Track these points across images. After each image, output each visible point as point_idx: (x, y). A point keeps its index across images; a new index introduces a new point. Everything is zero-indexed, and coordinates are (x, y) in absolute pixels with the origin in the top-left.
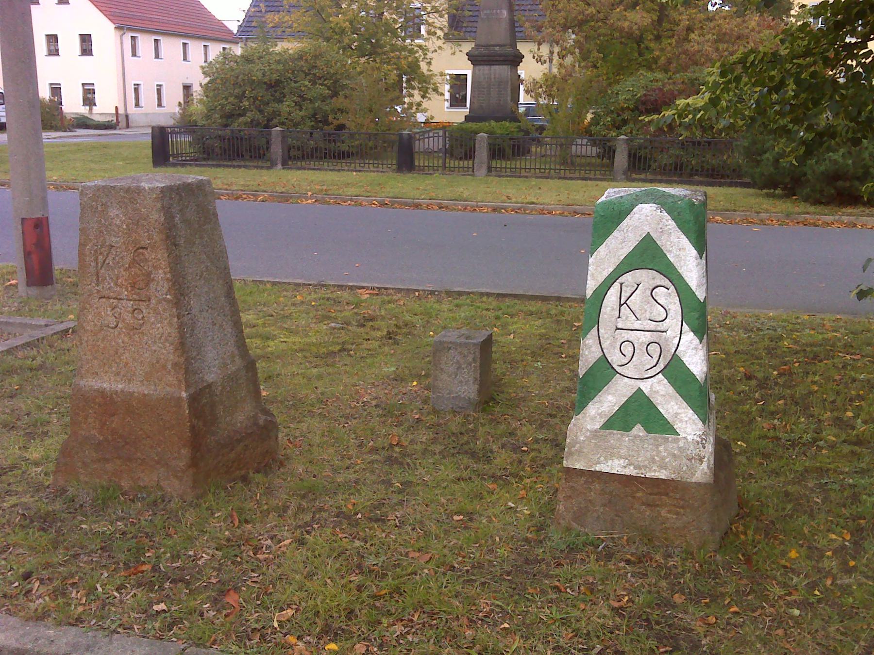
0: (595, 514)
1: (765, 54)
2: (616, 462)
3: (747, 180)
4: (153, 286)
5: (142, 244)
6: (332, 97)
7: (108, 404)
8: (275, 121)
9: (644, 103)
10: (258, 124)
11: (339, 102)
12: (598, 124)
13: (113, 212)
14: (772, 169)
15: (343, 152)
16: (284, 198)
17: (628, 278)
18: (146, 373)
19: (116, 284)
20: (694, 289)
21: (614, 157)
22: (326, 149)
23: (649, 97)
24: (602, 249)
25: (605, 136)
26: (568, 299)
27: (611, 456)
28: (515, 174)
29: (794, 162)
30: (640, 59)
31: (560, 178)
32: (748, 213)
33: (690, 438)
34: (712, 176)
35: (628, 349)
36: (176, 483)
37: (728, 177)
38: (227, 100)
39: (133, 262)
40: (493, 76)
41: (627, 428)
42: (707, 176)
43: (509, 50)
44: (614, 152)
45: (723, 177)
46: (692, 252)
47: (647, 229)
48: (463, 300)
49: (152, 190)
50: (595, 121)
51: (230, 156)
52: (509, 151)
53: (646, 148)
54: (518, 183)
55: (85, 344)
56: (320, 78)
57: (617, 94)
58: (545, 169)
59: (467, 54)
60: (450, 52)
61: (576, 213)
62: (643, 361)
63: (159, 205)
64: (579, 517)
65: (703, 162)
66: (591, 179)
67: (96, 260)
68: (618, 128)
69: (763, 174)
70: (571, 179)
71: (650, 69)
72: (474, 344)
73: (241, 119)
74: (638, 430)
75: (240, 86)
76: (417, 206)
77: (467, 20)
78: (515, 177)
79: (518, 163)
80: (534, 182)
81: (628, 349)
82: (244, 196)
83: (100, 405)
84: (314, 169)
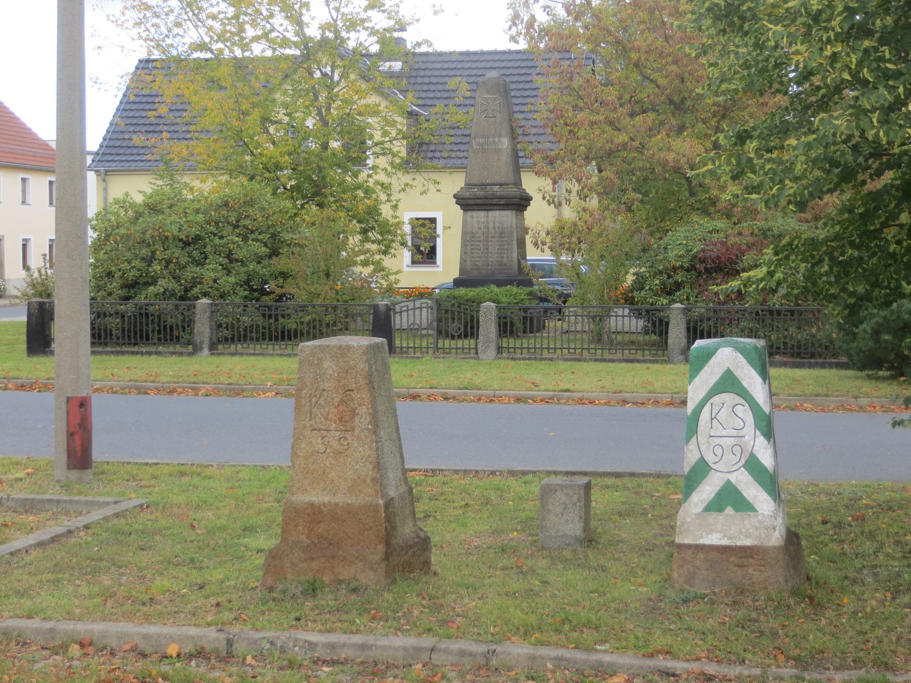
0: (701, 577)
1: (806, 240)
2: (715, 535)
3: (844, 359)
4: (357, 419)
5: (350, 387)
6: (270, 257)
7: (315, 514)
8: (196, 291)
9: (702, 261)
10: (173, 294)
11: (281, 263)
12: (643, 288)
13: (327, 364)
14: (871, 344)
15: (289, 331)
16: (236, 391)
18: (349, 487)
19: (326, 419)
20: (761, 405)
21: (667, 332)
22: (264, 328)
23: (708, 254)
24: (697, 380)
25: (652, 304)
26: (643, 475)
27: (711, 532)
28: (535, 355)
29: (841, 321)
30: (692, 200)
31: (596, 360)
32: (844, 399)
33: (766, 513)
34: (798, 355)
35: (719, 451)
36: (372, 575)
37: (820, 356)
38: (129, 263)
39: (342, 402)
40: (491, 225)
41: (721, 509)
42: (792, 355)
43: (512, 191)
44: (667, 324)
45: (812, 356)
46: (758, 379)
47: (727, 365)
48: (529, 478)
49: (360, 347)
50: (639, 284)
51: (129, 338)
52: (519, 325)
53: (709, 319)
54: (542, 367)
55: (297, 467)
56: (252, 232)
57: (665, 248)
58: (575, 349)
59: (455, 196)
60: (420, 188)
61: (625, 402)
63: (365, 358)
64: (689, 580)
65: (785, 337)
66: (638, 361)
67: (310, 401)
68: (669, 293)
69: (860, 350)
70: (613, 361)
71: (705, 212)
72: (579, 486)
73: (151, 288)
74: (729, 510)
75: (149, 245)
76: (415, 397)
77: (448, 148)
78: (535, 359)
79: (532, 341)
80: (562, 365)
81: (719, 451)
82: (180, 390)
83: (309, 515)
84: (254, 354)
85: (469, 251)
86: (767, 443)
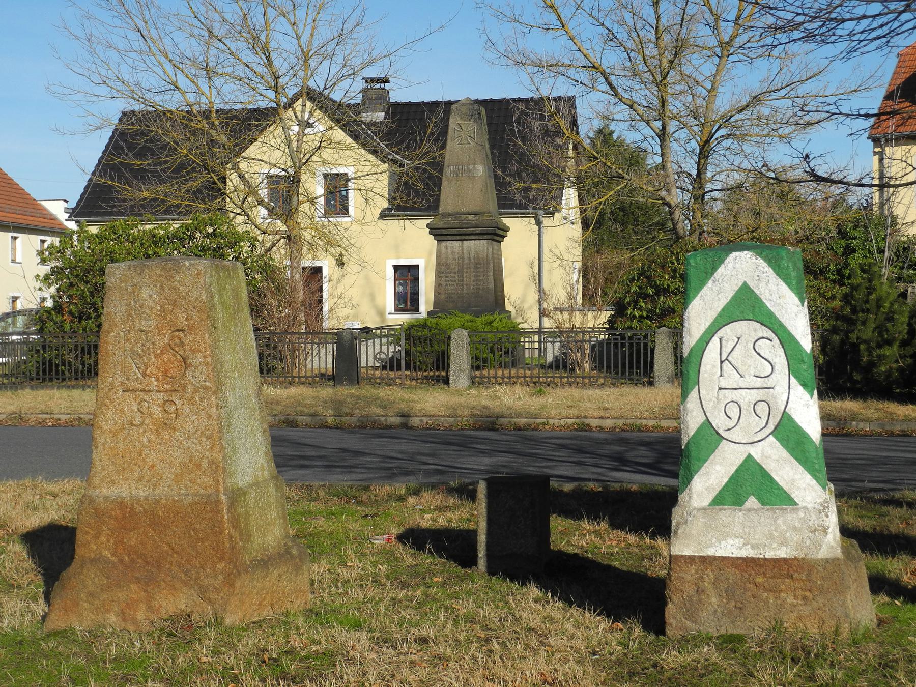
2: (730, 541)
13: (145, 293)
17: (728, 332)
19: (144, 374)
27: (724, 536)
33: (810, 506)
35: (734, 411)
41: (738, 502)
62: (753, 423)
74: (752, 502)
81: (734, 411)
85: (443, 283)
86: (808, 396)
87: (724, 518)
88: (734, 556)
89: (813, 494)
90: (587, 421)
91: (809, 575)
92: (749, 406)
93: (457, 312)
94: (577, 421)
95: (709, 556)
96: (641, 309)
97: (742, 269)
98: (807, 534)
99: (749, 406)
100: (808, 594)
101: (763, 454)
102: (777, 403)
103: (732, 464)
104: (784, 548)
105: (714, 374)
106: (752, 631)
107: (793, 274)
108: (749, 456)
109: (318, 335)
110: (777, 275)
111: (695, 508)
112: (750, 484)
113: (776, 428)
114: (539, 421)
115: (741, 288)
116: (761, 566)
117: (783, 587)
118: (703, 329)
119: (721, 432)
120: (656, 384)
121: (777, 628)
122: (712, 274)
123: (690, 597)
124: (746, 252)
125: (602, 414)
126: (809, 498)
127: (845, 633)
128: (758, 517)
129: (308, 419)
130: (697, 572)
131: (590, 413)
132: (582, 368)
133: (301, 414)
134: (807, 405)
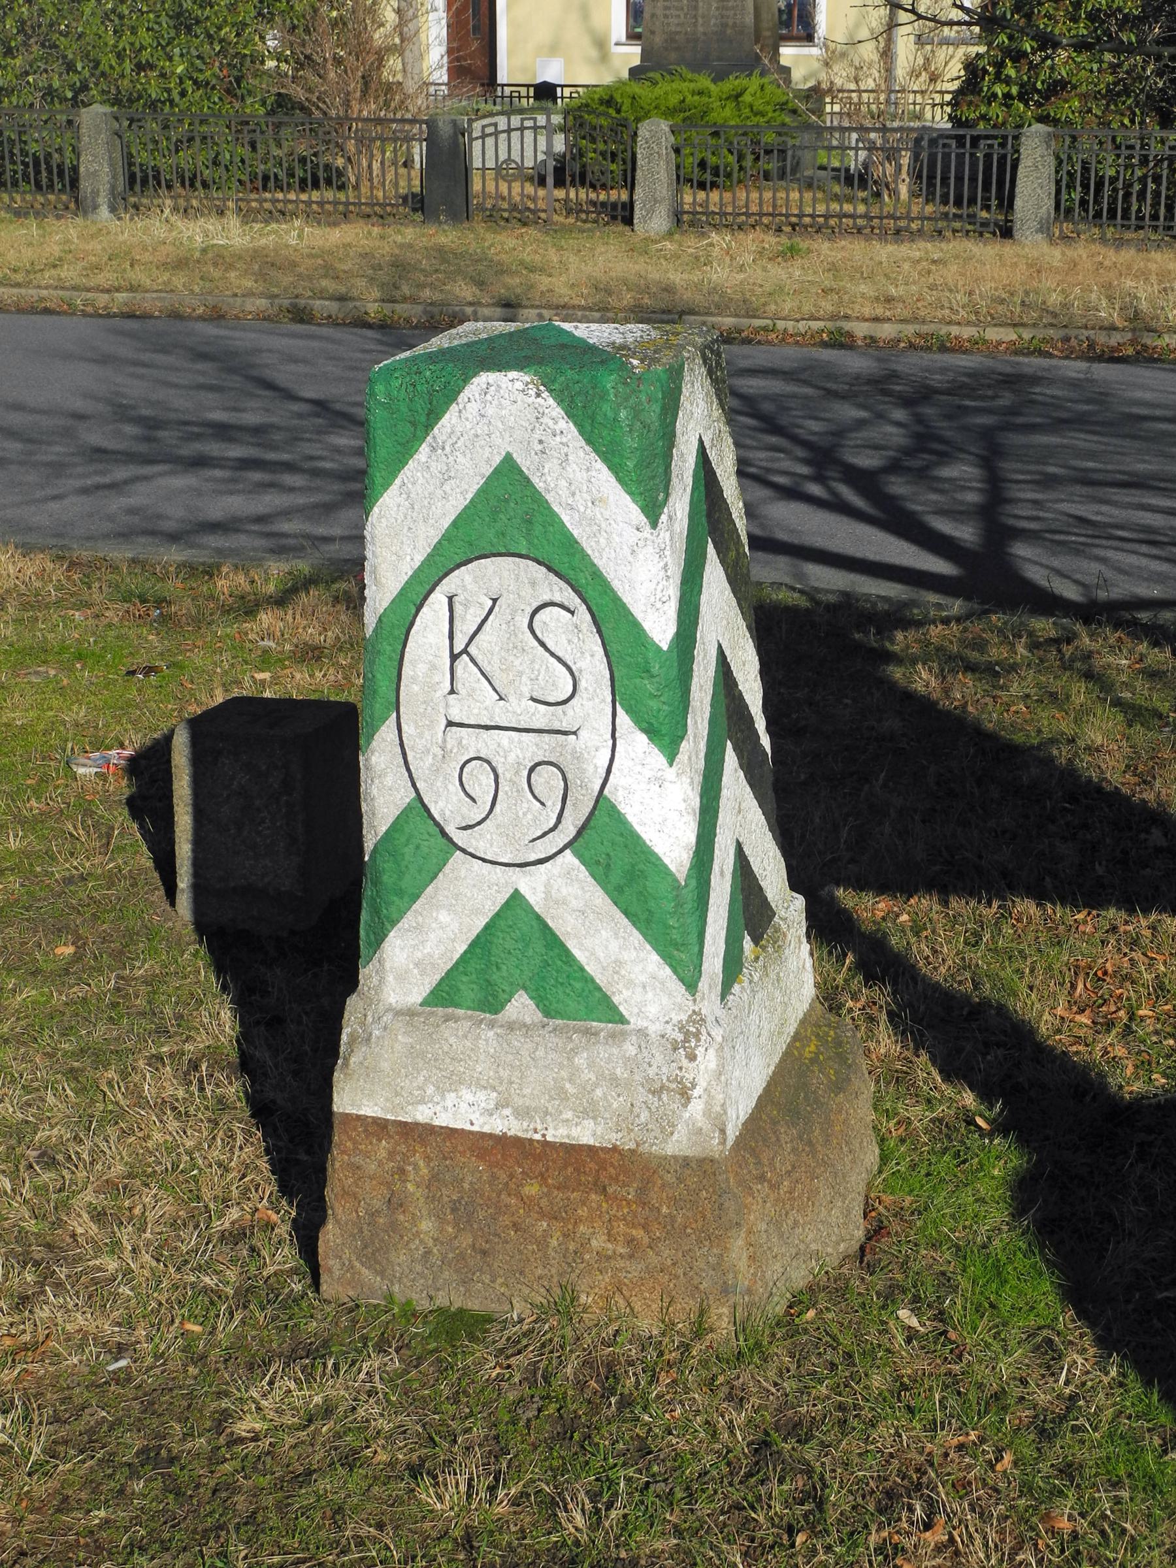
2: (467, 1095)
17: (463, 580)
27: (454, 1082)
33: (654, 1029)
62: (526, 817)
74: (521, 1006)
87: (452, 1040)
88: (475, 1128)
89: (665, 1000)
90: (847, 326)
91: (642, 1191)
92: (517, 773)
93: (684, 70)
94: (830, 325)
95: (417, 1124)
96: (1008, 81)
97: (502, 419)
98: (642, 1095)
99: (517, 773)
100: (638, 1233)
101: (547, 893)
102: (584, 771)
103: (476, 912)
104: (589, 1124)
105: (434, 687)
106: (507, 1307)
107: (631, 442)
108: (517, 896)
109: (386, 130)
110: (589, 442)
111: (389, 1009)
112: (516, 962)
113: (579, 833)
114: (757, 323)
115: (497, 471)
116: (538, 1158)
117: (583, 1212)
118: (406, 570)
119: (450, 830)
120: (1017, 234)
121: (564, 1306)
122: (429, 427)
123: (374, 1214)
124: (513, 374)
125: (879, 311)
126: (653, 1010)
127: (722, 1321)
128: (530, 1045)
129: (332, 307)
130: (392, 1154)
131: (856, 310)
132: (894, 193)
133: (322, 295)
134: (661, 782)
